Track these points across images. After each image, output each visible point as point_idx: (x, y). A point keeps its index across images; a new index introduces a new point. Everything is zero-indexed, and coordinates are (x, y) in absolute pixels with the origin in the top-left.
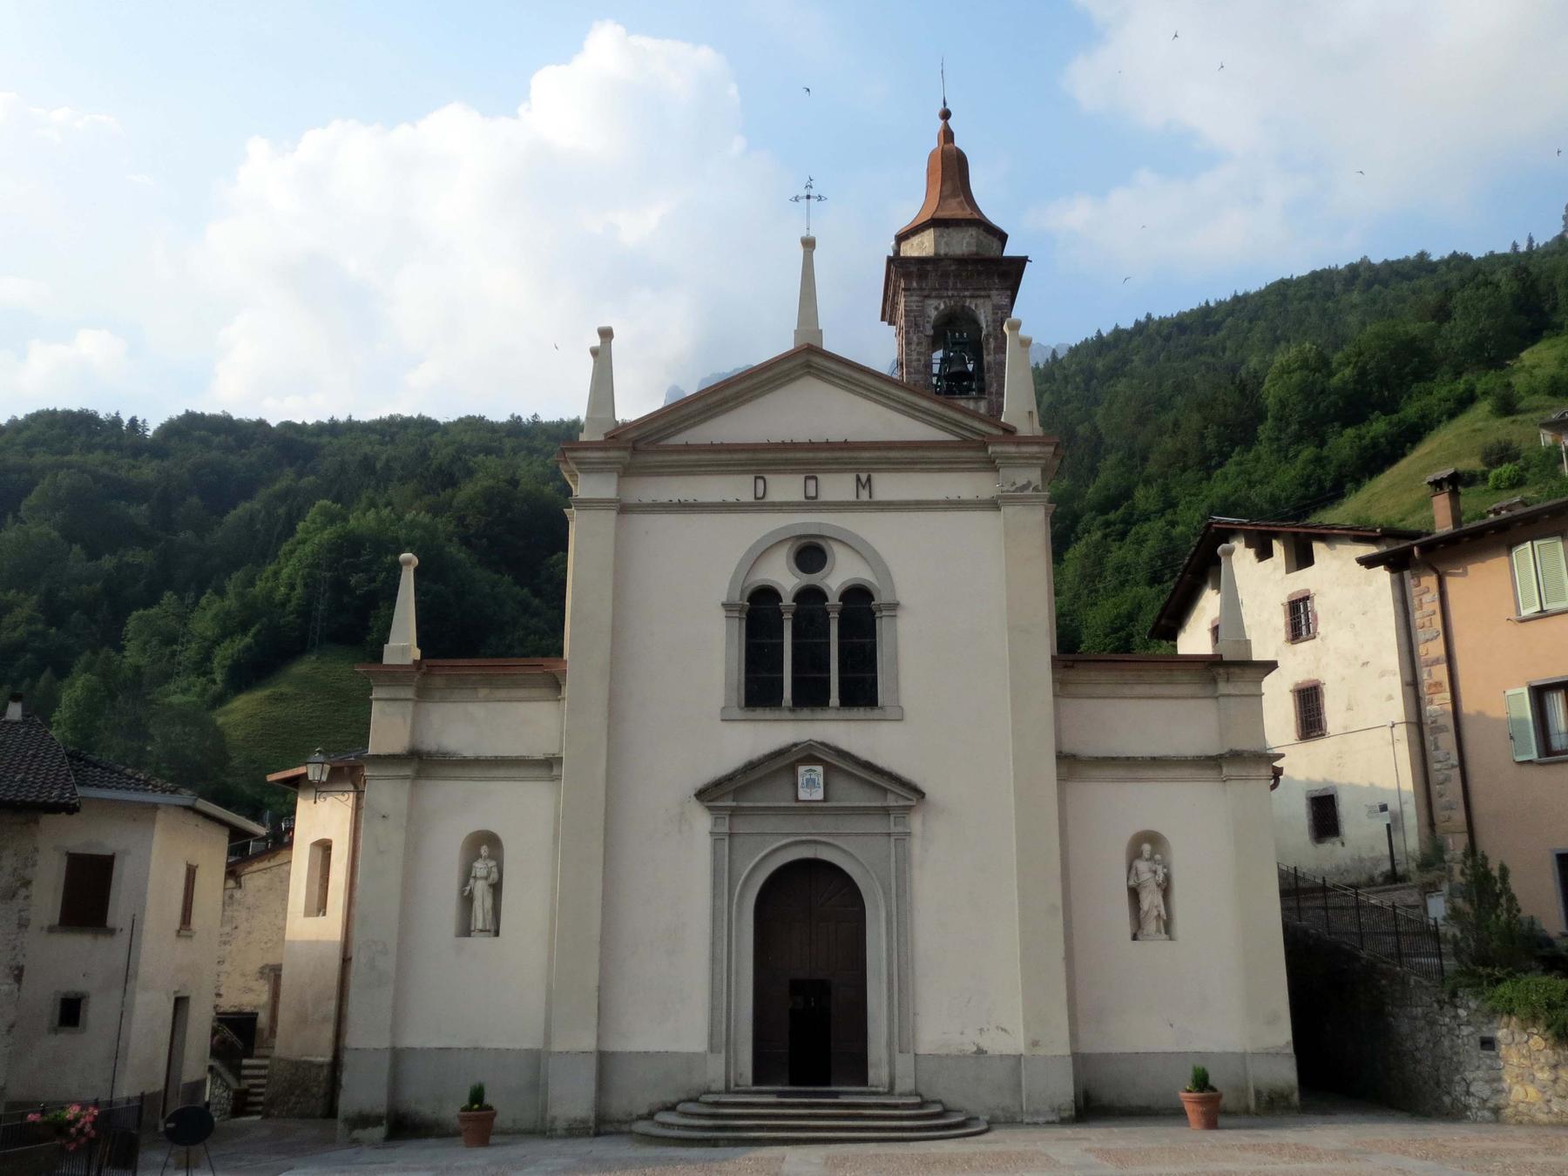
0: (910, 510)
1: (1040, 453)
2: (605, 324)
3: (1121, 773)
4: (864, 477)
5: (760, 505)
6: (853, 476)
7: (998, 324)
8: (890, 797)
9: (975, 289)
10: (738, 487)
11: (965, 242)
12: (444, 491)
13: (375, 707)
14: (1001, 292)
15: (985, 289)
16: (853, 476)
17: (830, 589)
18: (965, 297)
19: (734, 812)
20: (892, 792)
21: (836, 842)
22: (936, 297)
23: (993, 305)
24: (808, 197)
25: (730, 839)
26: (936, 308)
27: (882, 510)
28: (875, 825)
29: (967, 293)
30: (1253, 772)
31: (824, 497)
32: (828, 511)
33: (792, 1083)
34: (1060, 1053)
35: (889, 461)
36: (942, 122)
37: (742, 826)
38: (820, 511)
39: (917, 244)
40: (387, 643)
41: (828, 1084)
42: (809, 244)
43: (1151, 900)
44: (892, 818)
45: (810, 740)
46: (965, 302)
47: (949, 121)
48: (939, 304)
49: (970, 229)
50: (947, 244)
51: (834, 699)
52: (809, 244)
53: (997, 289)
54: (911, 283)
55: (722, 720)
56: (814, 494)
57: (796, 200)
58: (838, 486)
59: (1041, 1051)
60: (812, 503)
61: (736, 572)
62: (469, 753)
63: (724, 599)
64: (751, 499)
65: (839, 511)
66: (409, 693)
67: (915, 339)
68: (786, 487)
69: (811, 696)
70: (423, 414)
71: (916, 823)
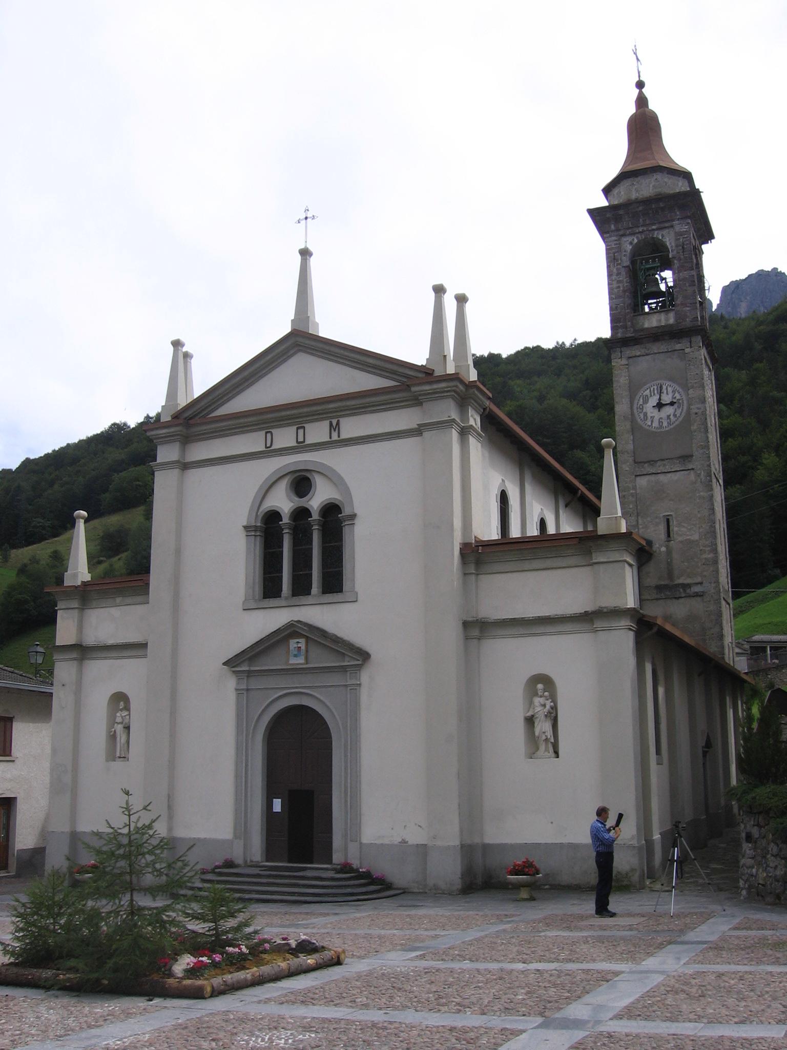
0: (363, 443)
1: (447, 387)
2: (460, 292)
3: (522, 631)
4: (334, 422)
5: (269, 452)
6: (327, 423)
7: (681, 248)
8: (347, 659)
9: (660, 223)
10: (252, 442)
11: (651, 186)
12: (724, 369)
13: (59, 613)
14: (682, 222)
15: (669, 221)
16: (327, 423)
17: (313, 508)
18: (653, 230)
19: (249, 674)
20: (347, 655)
21: (312, 693)
22: (631, 234)
23: (676, 233)
24: (306, 218)
25: (247, 693)
26: (631, 243)
27: (346, 445)
28: (335, 679)
29: (654, 227)
30: (615, 624)
31: (309, 441)
32: (310, 451)
33: (290, 861)
34: (452, 844)
35: (348, 408)
36: (638, 91)
37: (255, 683)
38: (307, 451)
39: (617, 194)
40: (67, 572)
41: (311, 863)
42: (305, 253)
43: (543, 727)
44: (348, 674)
45: (292, 621)
46: (653, 234)
47: (643, 90)
48: (633, 240)
49: (654, 174)
50: (637, 191)
51: (316, 588)
52: (305, 253)
53: (678, 219)
54: (610, 227)
55: (244, 610)
56: (302, 440)
57: (299, 222)
58: (317, 432)
59: (439, 843)
60: (301, 447)
61: (253, 502)
62: (111, 642)
63: (245, 524)
64: (294, 444)
65: (317, 450)
66: (75, 604)
67: (615, 270)
68: (285, 437)
69: (301, 588)
70: (492, 352)
71: (365, 676)
